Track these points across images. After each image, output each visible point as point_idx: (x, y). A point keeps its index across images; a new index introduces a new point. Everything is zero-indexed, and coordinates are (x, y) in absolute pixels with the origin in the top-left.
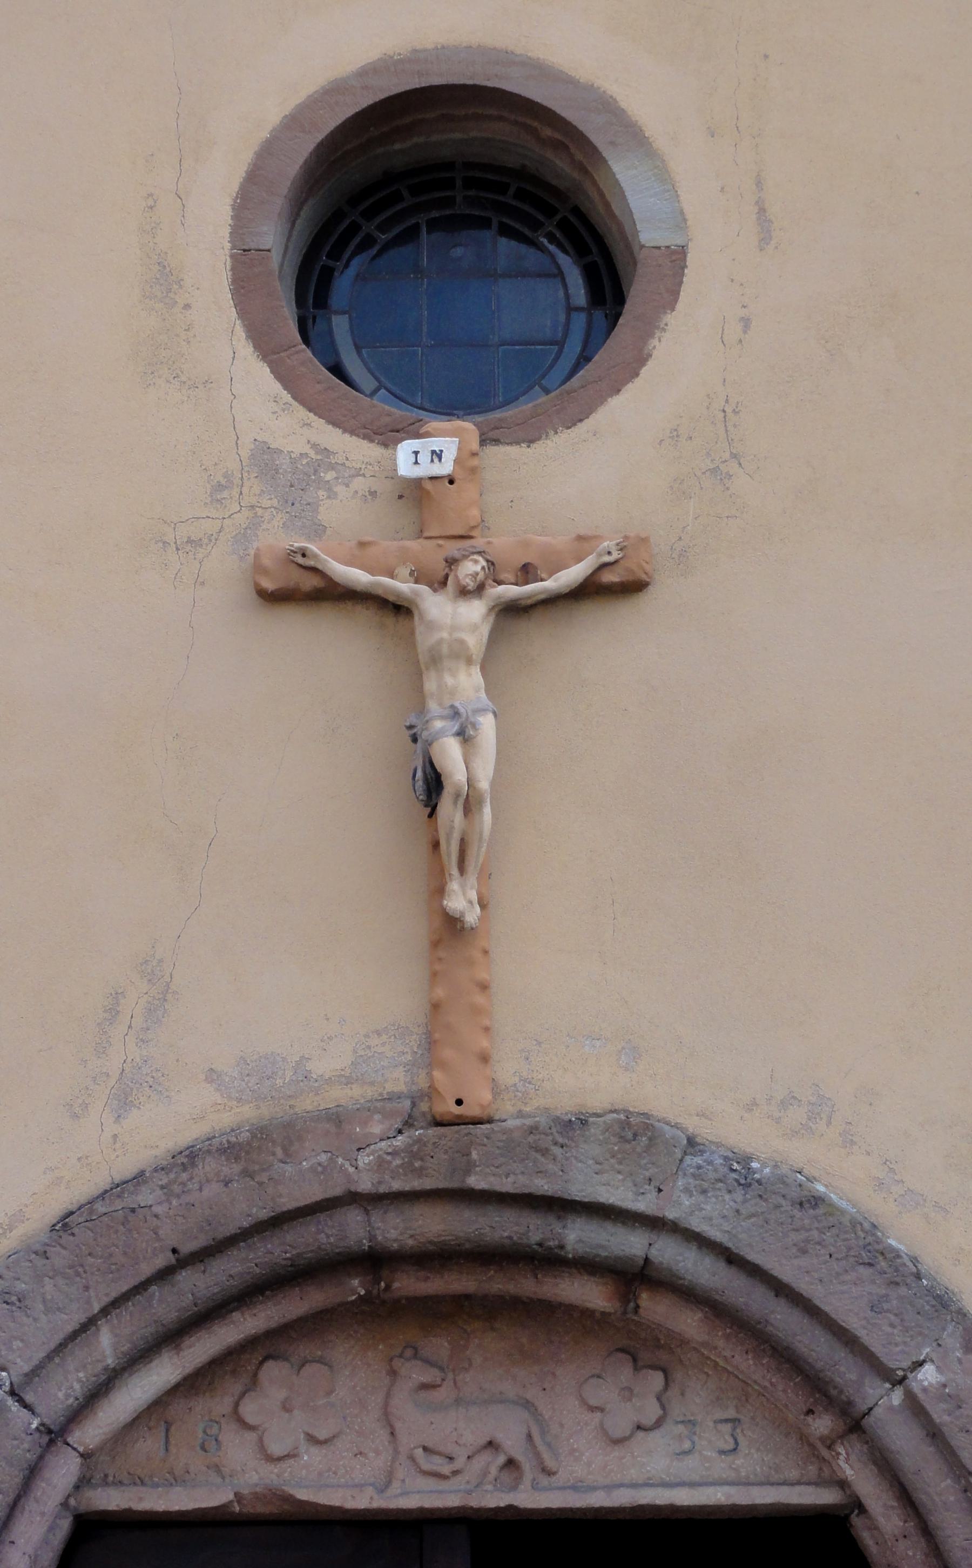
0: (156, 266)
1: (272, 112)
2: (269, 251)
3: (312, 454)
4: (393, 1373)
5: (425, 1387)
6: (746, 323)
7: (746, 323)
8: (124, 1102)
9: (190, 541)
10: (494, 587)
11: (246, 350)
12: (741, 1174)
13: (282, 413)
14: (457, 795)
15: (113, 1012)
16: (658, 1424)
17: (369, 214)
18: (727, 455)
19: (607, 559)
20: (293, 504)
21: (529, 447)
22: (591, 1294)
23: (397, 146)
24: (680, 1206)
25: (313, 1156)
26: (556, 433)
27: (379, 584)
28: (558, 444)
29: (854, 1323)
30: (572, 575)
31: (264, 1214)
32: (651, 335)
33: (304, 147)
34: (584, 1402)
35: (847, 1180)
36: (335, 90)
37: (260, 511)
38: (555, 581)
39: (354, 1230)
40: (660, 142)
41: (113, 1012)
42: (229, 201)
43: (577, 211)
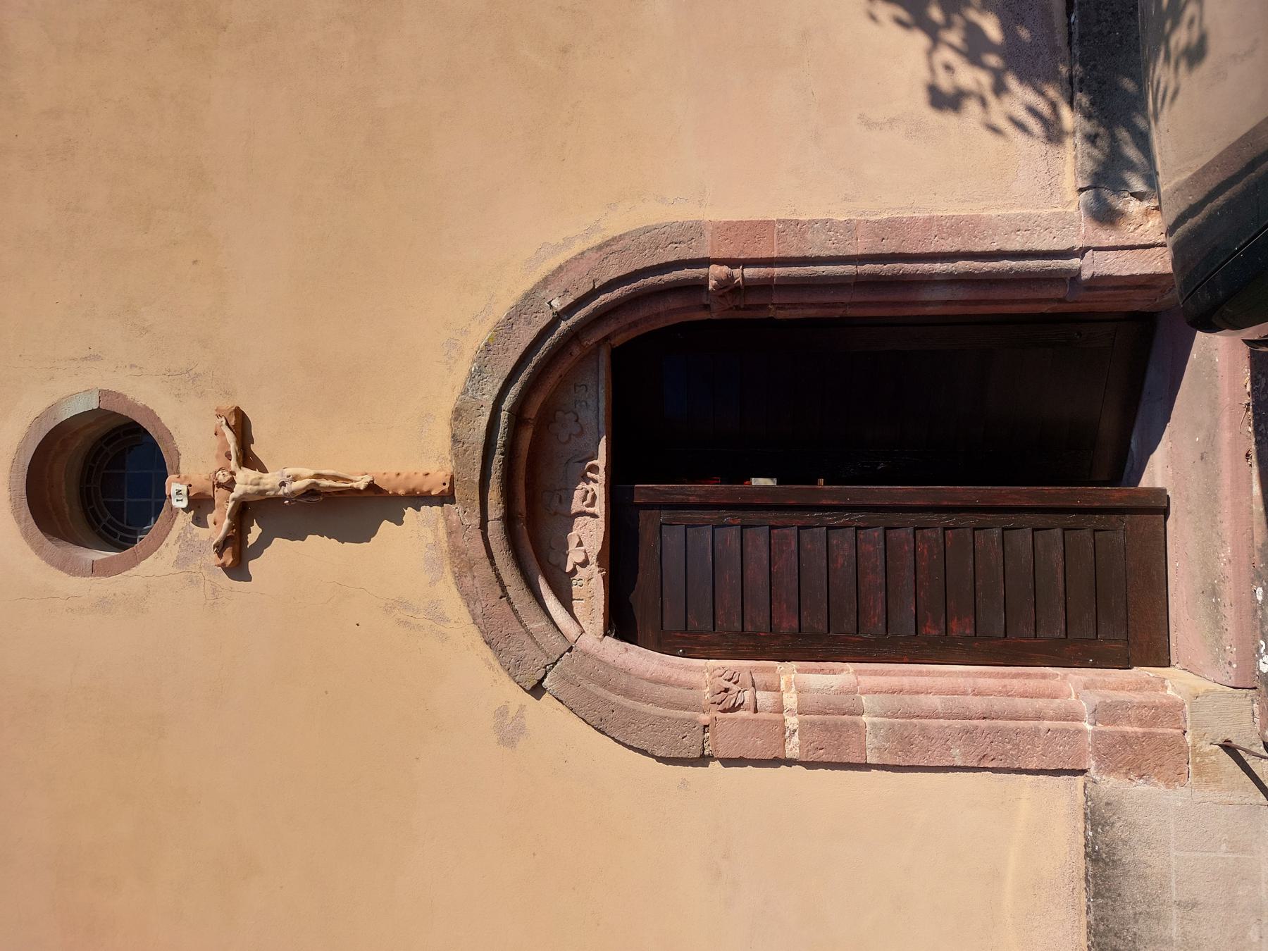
4: (556, 514)
5: (560, 501)
6: (132, 366)
7: (132, 366)
8: (443, 619)
11: (134, 570)
12: (477, 375)
15: (406, 623)
16: (576, 414)
17: (99, 521)
22: (527, 435)
23: (67, 509)
24: (489, 400)
25: (463, 543)
28: (178, 442)
29: (534, 332)
30: (230, 437)
31: (487, 563)
33: (49, 545)
34: (567, 442)
35: (481, 333)
36: (26, 535)
39: (495, 527)
40: (55, 399)
41: (406, 623)
43: (102, 439)
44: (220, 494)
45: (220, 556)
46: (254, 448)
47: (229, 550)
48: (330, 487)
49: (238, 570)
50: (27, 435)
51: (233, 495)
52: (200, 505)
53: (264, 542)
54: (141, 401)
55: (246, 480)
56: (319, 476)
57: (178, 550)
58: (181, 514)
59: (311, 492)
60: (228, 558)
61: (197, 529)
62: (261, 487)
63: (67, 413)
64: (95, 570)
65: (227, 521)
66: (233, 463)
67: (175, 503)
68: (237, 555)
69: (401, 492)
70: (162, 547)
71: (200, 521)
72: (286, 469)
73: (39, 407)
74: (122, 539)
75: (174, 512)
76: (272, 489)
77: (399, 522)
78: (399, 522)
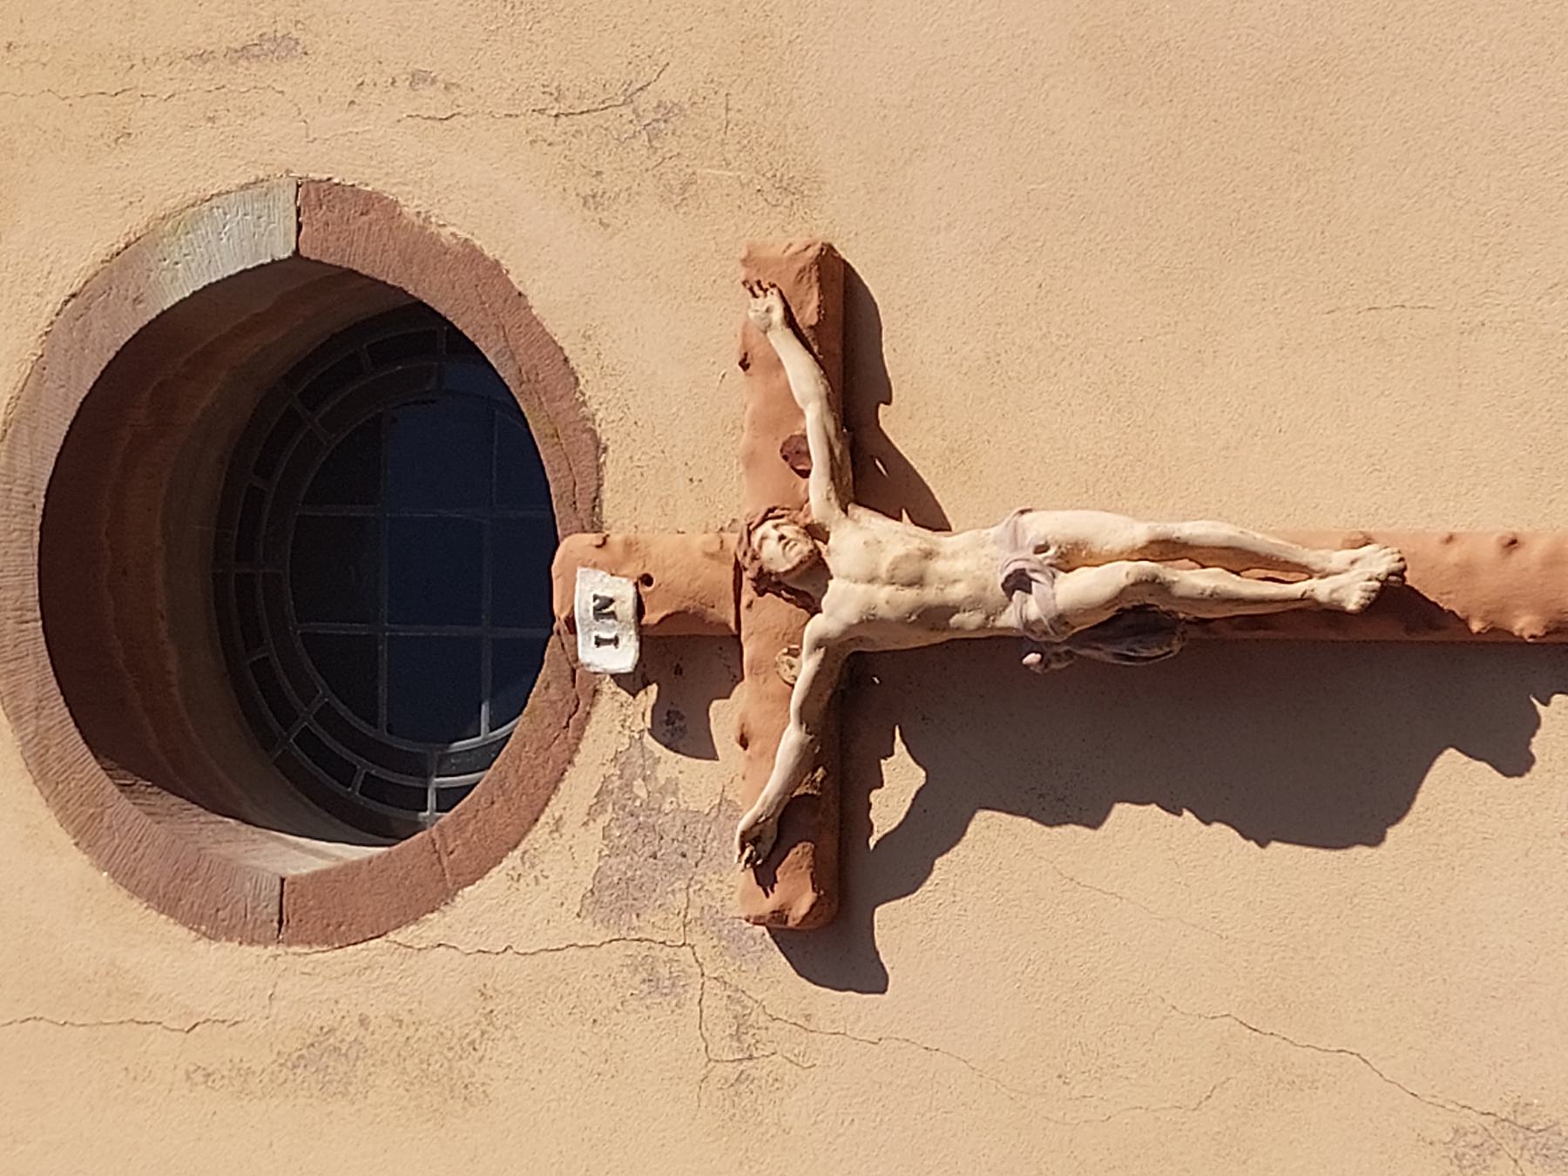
0: (299, 1071)
1: (72, 865)
2: (283, 880)
3: (603, 820)
6: (418, 79)
7: (418, 79)
9: (737, 1036)
10: (809, 509)
11: (435, 925)
13: (538, 868)
14: (929, 555)
18: (627, 111)
19: (778, 314)
20: (684, 856)
21: (605, 450)
23: (172, 664)
26: (584, 403)
27: (802, 709)
28: (602, 401)
30: (801, 374)
32: (434, 239)
33: (131, 814)
36: (41, 767)
37: (693, 913)
38: (806, 402)
40: (136, 221)
42: (202, 945)
44: (764, 616)
45: (766, 880)
46: (889, 420)
47: (799, 856)
48: (1218, 599)
49: (832, 945)
50: (40, 365)
51: (819, 625)
52: (685, 661)
53: (934, 827)
54: (456, 222)
55: (868, 563)
56: (1168, 549)
57: (609, 842)
58: (611, 700)
59: (1138, 618)
60: (797, 893)
61: (672, 764)
62: (931, 595)
63: (177, 283)
64: (295, 917)
65: (792, 736)
66: (818, 487)
67: (591, 656)
68: (830, 885)
69: (1525, 624)
70: (539, 833)
71: (681, 729)
72: (1029, 519)
73: (77, 256)
74: (375, 788)
75: (583, 686)
76: (974, 603)
77: (1513, 759)
78: (1513, 759)
